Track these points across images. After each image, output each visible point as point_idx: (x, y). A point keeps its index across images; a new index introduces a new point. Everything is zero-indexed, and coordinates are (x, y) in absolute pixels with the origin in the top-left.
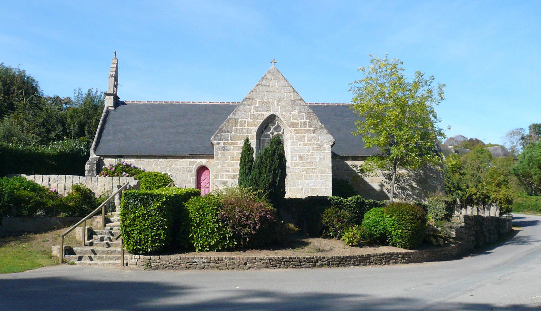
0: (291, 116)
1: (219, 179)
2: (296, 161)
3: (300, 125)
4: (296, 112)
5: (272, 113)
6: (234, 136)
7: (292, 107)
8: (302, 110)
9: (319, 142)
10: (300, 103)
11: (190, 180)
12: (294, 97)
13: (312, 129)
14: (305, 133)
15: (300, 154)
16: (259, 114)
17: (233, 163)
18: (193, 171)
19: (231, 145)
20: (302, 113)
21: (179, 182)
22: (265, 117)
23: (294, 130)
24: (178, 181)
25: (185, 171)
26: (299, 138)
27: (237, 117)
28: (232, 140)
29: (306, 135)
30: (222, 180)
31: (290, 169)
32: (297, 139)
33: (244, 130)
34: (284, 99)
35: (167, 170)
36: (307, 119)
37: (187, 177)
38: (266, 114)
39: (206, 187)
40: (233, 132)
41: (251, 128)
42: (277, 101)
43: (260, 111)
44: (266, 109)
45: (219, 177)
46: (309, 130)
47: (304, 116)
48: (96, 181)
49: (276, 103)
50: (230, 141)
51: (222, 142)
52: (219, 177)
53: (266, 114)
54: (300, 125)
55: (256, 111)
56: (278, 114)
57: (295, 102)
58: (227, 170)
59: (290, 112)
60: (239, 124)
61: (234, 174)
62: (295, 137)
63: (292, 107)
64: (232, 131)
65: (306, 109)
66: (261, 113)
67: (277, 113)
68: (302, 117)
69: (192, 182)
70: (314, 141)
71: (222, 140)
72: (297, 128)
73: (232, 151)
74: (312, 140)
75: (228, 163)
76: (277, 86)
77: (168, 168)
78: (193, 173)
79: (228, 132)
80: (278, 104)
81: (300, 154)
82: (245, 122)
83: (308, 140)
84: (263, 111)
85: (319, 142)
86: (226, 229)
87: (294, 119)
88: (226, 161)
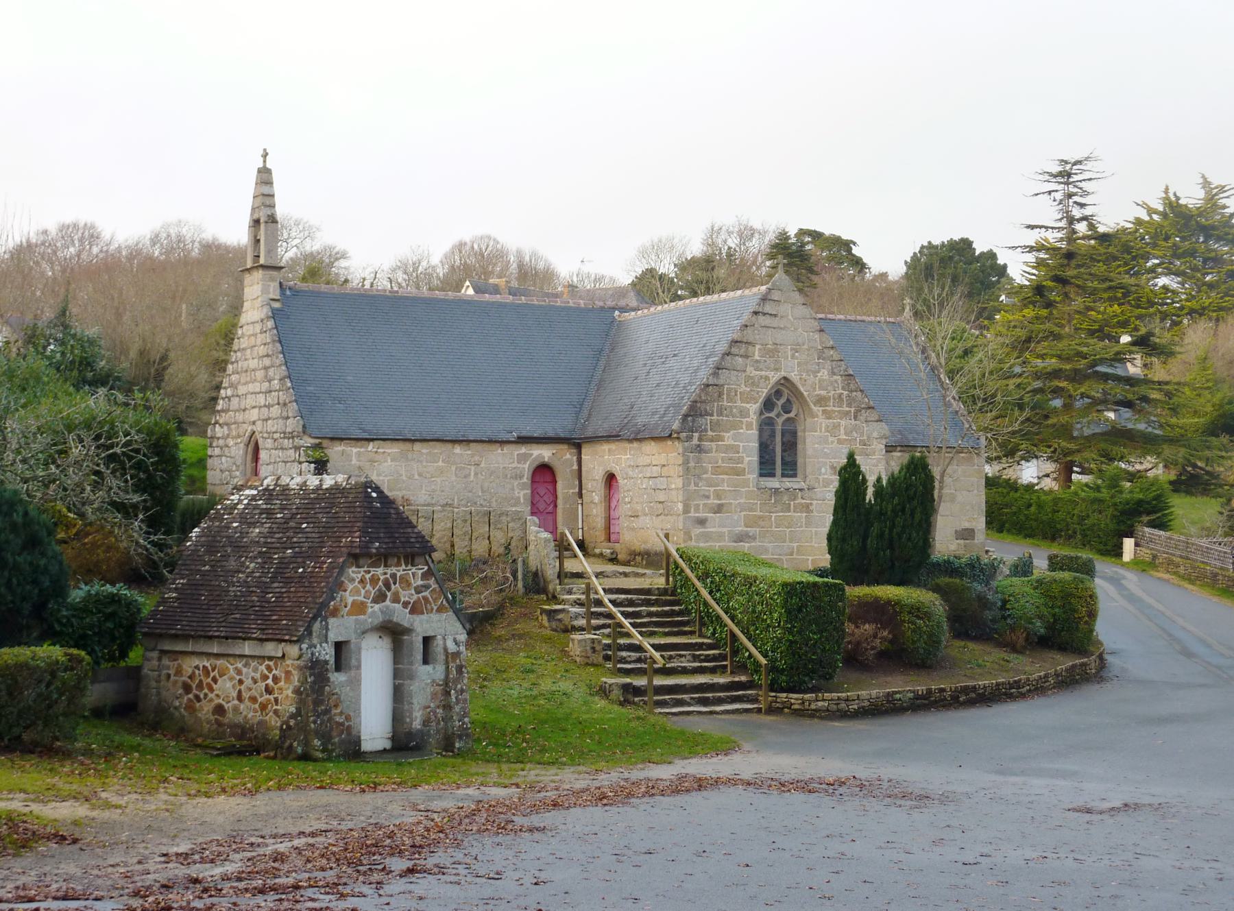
0: (817, 382)
1: (692, 514)
2: (826, 476)
3: (832, 401)
4: (824, 374)
5: (783, 374)
6: (718, 423)
7: (818, 364)
8: (835, 370)
9: (865, 438)
10: (832, 356)
11: (519, 498)
12: (822, 342)
13: (853, 410)
14: (841, 419)
15: (833, 460)
16: (761, 376)
17: (717, 479)
18: (526, 476)
19: (712, 441)
20: (835, 377)
21: (496, 501)
22: (771, 382)
23: (823, 411)
24: (494, 500)
25: (509, 476)
26: (830, 428)
27: (721, 382)
28: (714, 431)
29: (843, 422)
30: (697, 515)
31: (815, 492)
32: (828, 431)
33: (734, 410)
34: (804, 345)
35: (469, 475)
36: (843, 388)
37: (513, 490)
38: (773, 377)
39: (547, 511)
40: (715, 414)
41: (748, 406)
42: (792, 349)
43: (761, 370)
44: (772, 366)
45: (692, 510)
46: (848, 413)
47: (840, 382)
48: (429, 518)
49: (790, 353)
50: (710, 433)
51: (696, 435)
52: (692, 510)
53: (773, 377)
54: (832, 401)
55: (755, 370)
56: (794, 376)
57: (823, 352)
58: (707, 494)
59: (815, 373)
60: (725, 397)
61: (719, 502)
62: (823, 425)
63: (818, 364)
64: (713, 411)
65: (842, 369)
66: (763, 373)
67: (793, 374)
68: (836, 385)
69: (522, 501)
70: (856, 435)
71: (696, 432)
72: (827, 408)
73: (713, 454)
74: (852, 432)
75: (706, 479)
76: (790, 317)
77: (473, 468)
78: (525, 480)
79: (707, 414)
80: (793, 357)
81: (833, 460)
82: (736, 392)
83: (846, 434)
84: (768, 368)
85: (865, 438)
86: (257, 563)
87: (821, 388)
88: (704, 476)
